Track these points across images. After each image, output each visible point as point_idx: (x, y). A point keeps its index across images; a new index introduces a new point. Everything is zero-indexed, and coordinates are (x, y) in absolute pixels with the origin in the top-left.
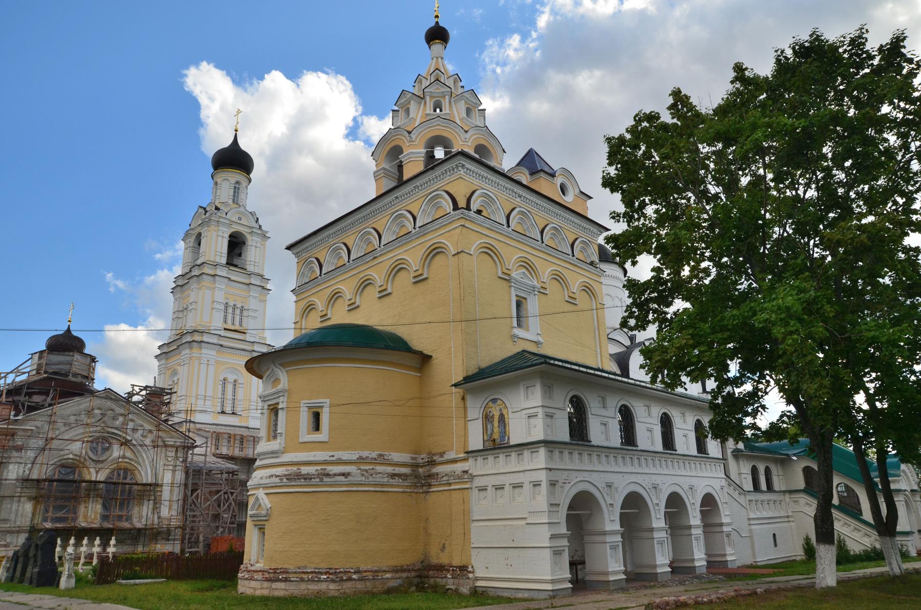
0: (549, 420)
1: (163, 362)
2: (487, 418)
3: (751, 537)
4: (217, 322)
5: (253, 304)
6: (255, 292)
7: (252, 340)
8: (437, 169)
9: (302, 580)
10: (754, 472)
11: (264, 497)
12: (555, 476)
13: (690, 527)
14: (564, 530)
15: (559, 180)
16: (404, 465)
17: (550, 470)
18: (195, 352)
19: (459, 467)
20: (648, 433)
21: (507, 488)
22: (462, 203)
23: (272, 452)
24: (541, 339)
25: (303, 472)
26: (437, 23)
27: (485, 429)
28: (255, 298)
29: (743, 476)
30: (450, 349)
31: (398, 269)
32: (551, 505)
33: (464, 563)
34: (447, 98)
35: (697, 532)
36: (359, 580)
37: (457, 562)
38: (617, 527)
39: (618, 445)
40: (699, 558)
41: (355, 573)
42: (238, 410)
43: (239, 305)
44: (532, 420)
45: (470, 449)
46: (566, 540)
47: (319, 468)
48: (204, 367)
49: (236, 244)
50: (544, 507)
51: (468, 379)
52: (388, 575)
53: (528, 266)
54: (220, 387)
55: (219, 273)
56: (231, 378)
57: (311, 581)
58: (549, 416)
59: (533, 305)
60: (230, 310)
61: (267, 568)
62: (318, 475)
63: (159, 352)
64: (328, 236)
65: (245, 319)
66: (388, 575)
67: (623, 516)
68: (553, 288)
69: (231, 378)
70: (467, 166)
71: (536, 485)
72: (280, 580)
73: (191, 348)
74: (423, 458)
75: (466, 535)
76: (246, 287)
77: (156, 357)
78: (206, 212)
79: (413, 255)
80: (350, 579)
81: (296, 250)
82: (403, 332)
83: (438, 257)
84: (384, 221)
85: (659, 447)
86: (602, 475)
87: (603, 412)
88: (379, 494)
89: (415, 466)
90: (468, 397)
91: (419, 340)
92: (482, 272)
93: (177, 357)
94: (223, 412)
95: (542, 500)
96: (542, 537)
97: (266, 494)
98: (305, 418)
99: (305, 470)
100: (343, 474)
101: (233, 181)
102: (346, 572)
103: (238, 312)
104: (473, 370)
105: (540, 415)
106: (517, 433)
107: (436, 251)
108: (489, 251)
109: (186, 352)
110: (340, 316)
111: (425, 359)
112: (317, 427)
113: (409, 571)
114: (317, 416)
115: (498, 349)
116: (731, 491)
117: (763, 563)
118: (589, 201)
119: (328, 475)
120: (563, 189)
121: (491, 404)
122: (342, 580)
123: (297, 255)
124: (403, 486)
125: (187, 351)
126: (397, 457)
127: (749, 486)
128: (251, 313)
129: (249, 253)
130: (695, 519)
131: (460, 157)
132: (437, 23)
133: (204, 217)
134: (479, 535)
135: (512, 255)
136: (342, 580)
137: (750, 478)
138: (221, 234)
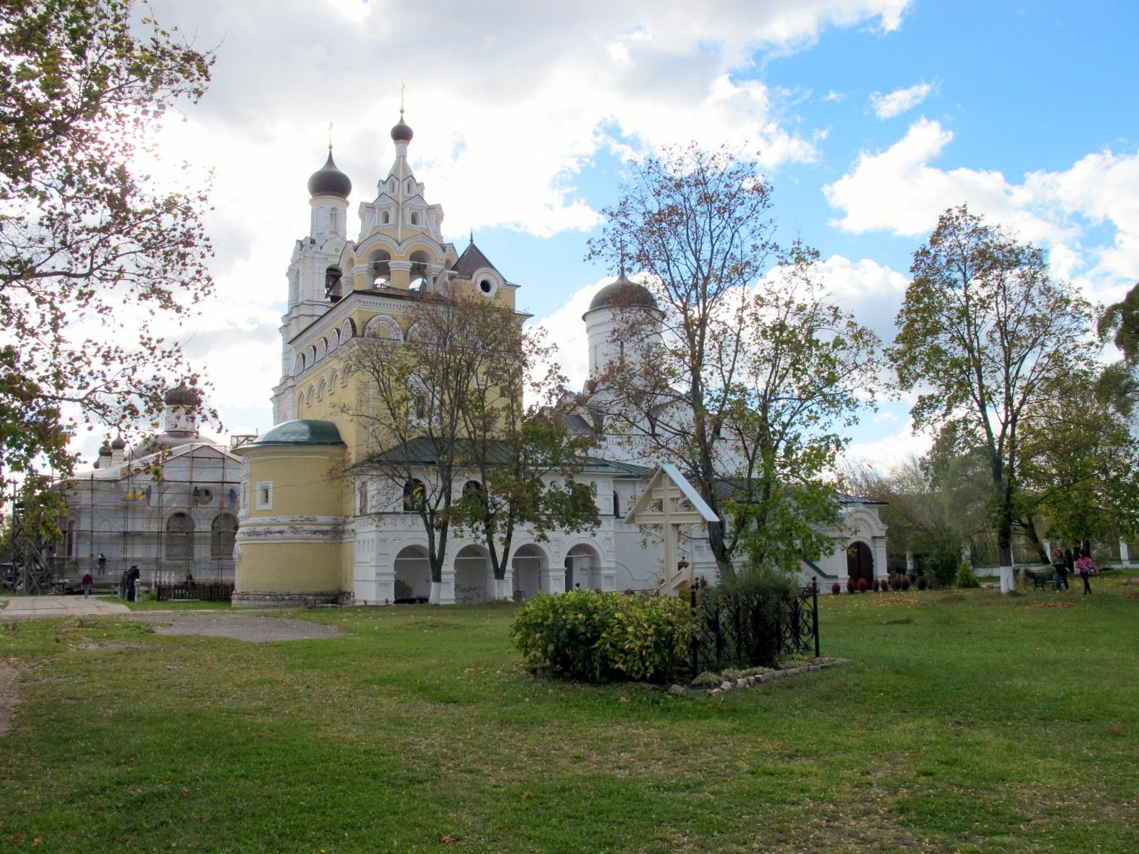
16: (328, 524)
26: (402, 120)
33: (425, 595)
57: (260, 600)
67: (397, 564)
80: (283, 599)
98: (259, 495)
99: (258, 529)
100: (280, 532)
101: (328, 207)
117: (444, 603)
119: (270, 533)
126: (321, 519)
132: (402, 120)
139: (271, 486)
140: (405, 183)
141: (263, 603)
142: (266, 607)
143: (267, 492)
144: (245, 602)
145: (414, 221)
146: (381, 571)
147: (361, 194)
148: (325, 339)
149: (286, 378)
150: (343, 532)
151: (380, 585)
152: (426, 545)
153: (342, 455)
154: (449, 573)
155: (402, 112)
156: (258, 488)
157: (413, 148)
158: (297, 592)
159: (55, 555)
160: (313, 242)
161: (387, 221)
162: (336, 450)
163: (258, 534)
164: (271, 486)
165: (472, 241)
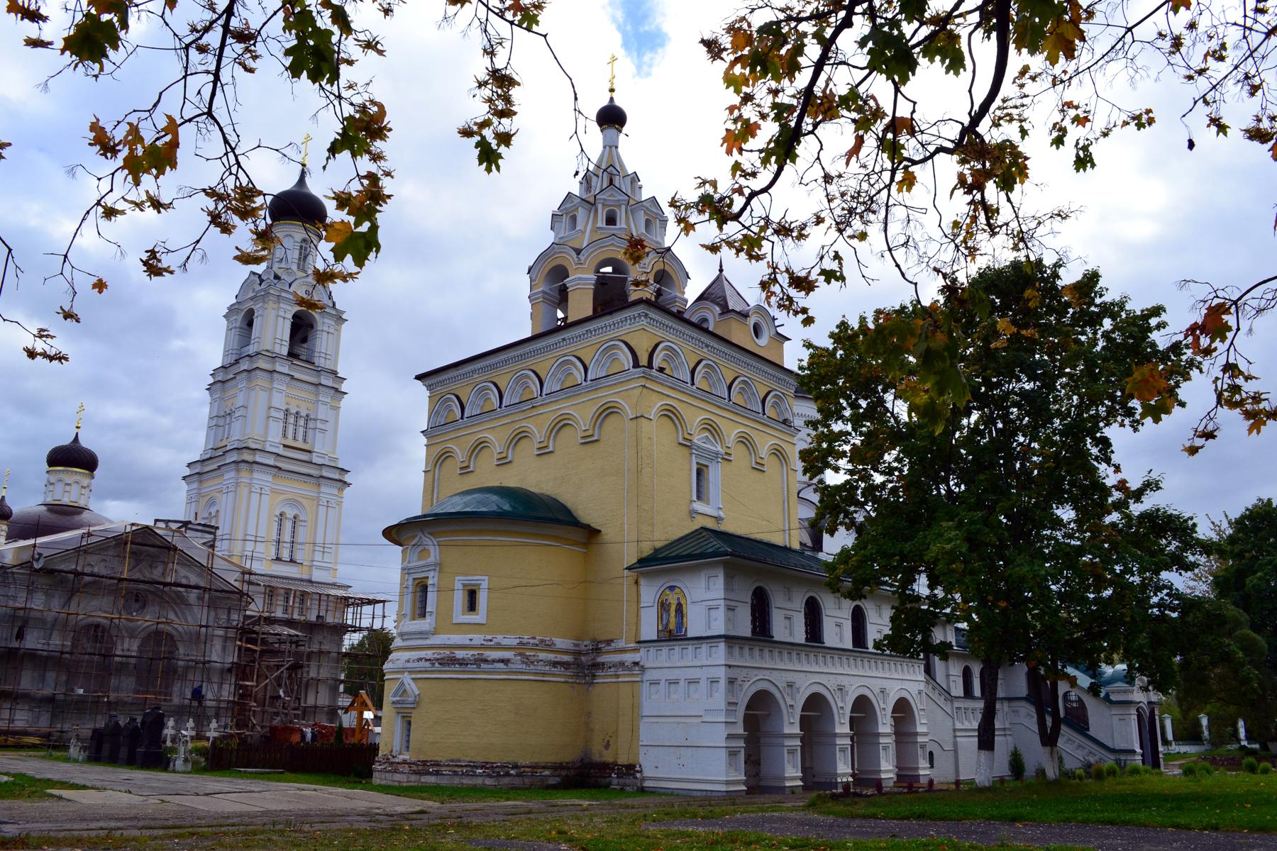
0: (731, 613)
1: (195, 485)
2: (663, 606)
3: (956, 751)
4: (274, 438)
5: (322, 412)
6: (325, 397)
7: (320, 461)
9: (455, 773)
10: (967, 674)
12: (734, 673)
13: (878, 735)
14: (741, 731)
15: (752, 320)
16: (566, 652)
17: (730, 666)
18: (245, 476)
19: (629, 658)
20: (837, 630)
21: (682, 683)
22: (644, 360)
23: (421, 633)
24: (721, 514)
26: (612, 99)
27: (660, 618)
28: (325, 403)
29: (952, 678)
30: (622, 524)
31: (562, 424)
33: (631, 761)
34: (623, 208)
35: (887, 741)
36: (518, 775)
37: (622, 760)
38: (796, 730)
39: (803, 641)
40: (887, 769)
42: (298, 557)
43: (303, 414)
44: (713, 612)
45: (642, 639)
48: (255, 497)
49: (302, 329)
50: (723, 706)
51: (643, 562)
53: (711, 429)
54: (275, 526)
55: (278, 368)
56: (290, 513)
58: (730, 609)
59: (715, 474)
60: (291, 420)
61: (413, 760)
63: (187, 472)
64: (473, 372)
65: (310, 432)
66: (547, 773)
68: (738, 453)
69: (290, 513)
70: (651, 315)
71: (714, 681)
72: (430, 774)
73: (238, 470)
74: (586, 644)
75: (634, 731)
76: (311, 388)
77: (184, 478)
78: (262, 281)
79: (582, 412)
80: (507, 774)
81: (429, 382)
82: (567, 496)
83: (613, 417)
84: (547, 364)
85: (848, 644)
86: (783, 674)
87: (788, 605)
90: (642, 582)
91: (587, 513)
92: (658, 435)
93: (216, 481)
94: (278, 559)
95: (720, 698)
96: (718, 736)
98: (460, 598)
99: (460, 654)
100: (502, 661)
102: (502, 767)
103: (302, 422)
104: (647, 550)
105: (722, 609)
106: (696, 625)
107: (608, 411)
108: (670, 414)
109: (230, 475)
110: (488, 474)
111: (591, 534)
112: (472, 606)
114: (472, 595)
115: (671, 526)
116: (935, 696)
118: (787, 344)
119: (486, 661)
120: (757, 330)
121: (668, 592)
122: (499, 775)
123: (429, 387)
125: (232, 474)
126: (561, 643)
127: (958, 690)
128: (319, 425)
129: (318, 341)
130: (885, 726)
132: (612, 99)
133: (258, 288)
134: (647, 733)
135: (694, 417)
136: (499, 775)
137: (960, 681)
138: (281, 313)
139: (485, 585)
143: (424, 589)
150: (597, 666)
154: (843, 736)
155: (612, 90)
156: (458, 585)
164: (485, 585)
165: (721, 270)
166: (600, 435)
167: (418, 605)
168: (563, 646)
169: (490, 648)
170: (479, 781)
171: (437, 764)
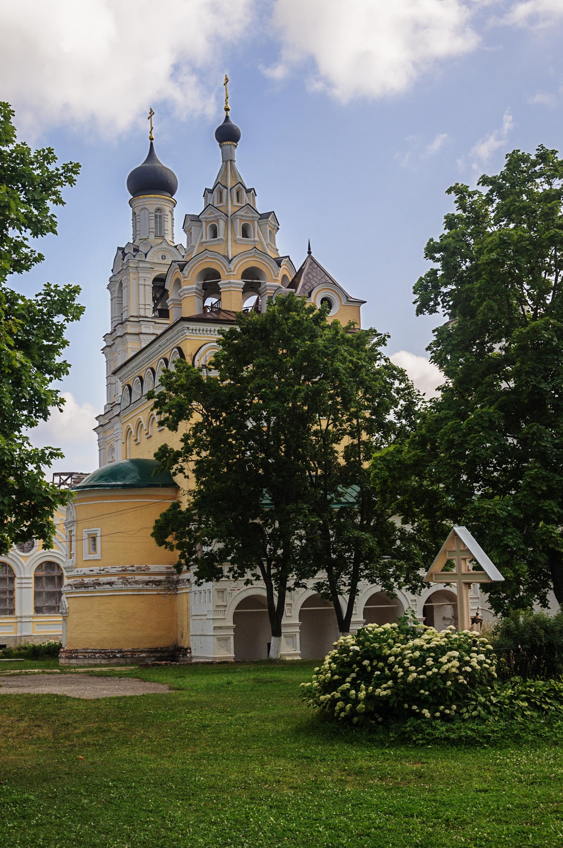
8: (174, 328)
11: (65, 600)
25: (85, 582)
26: (227, 117)
32: (217, 606)
36: (121, 657)
37: (186, 646)
41: (118, 652)
46: (232, 630)
47: (94, 579)
52: (144, 655)
62: (94, 584)
63: (97, 424)
66: (144, 655)
67: (235, 615)
72: (73, 658)
80: (115, 657)
81: (120, 374)
88: (136, 597)
89: (169, 574)
97: (67, 598)
98: (86, 544)
99: (86, 580)
102: (112, 652)
113: (162, 652)
119: (99, 584)
122: (109, 658)
124: (157, 590)
126: (154, 568)
131: (182, 323)
132: (227, 117)
136: (109, 658)
140: (234, 191)
141: (91, 662)
142: (96, 666)
143: (94, 539)
144: (73, 661)
145: (245, 234)
146: (218, 624)
147: (189, 200)
148: (152, 369)
149: (112, 405)
150: (178, 582)
151: (219, 640)
152: (265, 593)
153: (175, 498)
155: (227, 110)
156: (85, 536)
157: (239, 153)
158: (130, 649)
159: (541, 524)
160: (136, 250)
161: (215, 235)
162: (168, 492)
163: (85, 586)
164: (99, 534)
165: (309, 253)
166: (140, 439)
167: (91, 546)
168: (157, 570)
169: (104, 575)
170: (98, 661)
171: (76, 651)
